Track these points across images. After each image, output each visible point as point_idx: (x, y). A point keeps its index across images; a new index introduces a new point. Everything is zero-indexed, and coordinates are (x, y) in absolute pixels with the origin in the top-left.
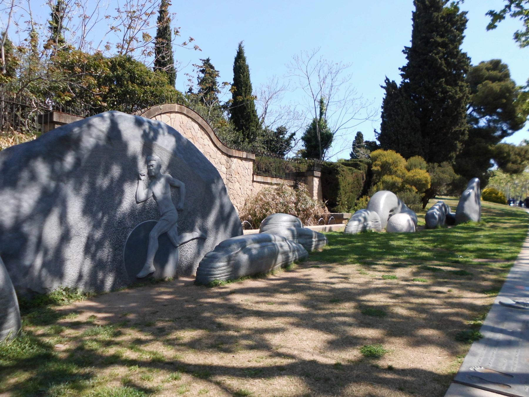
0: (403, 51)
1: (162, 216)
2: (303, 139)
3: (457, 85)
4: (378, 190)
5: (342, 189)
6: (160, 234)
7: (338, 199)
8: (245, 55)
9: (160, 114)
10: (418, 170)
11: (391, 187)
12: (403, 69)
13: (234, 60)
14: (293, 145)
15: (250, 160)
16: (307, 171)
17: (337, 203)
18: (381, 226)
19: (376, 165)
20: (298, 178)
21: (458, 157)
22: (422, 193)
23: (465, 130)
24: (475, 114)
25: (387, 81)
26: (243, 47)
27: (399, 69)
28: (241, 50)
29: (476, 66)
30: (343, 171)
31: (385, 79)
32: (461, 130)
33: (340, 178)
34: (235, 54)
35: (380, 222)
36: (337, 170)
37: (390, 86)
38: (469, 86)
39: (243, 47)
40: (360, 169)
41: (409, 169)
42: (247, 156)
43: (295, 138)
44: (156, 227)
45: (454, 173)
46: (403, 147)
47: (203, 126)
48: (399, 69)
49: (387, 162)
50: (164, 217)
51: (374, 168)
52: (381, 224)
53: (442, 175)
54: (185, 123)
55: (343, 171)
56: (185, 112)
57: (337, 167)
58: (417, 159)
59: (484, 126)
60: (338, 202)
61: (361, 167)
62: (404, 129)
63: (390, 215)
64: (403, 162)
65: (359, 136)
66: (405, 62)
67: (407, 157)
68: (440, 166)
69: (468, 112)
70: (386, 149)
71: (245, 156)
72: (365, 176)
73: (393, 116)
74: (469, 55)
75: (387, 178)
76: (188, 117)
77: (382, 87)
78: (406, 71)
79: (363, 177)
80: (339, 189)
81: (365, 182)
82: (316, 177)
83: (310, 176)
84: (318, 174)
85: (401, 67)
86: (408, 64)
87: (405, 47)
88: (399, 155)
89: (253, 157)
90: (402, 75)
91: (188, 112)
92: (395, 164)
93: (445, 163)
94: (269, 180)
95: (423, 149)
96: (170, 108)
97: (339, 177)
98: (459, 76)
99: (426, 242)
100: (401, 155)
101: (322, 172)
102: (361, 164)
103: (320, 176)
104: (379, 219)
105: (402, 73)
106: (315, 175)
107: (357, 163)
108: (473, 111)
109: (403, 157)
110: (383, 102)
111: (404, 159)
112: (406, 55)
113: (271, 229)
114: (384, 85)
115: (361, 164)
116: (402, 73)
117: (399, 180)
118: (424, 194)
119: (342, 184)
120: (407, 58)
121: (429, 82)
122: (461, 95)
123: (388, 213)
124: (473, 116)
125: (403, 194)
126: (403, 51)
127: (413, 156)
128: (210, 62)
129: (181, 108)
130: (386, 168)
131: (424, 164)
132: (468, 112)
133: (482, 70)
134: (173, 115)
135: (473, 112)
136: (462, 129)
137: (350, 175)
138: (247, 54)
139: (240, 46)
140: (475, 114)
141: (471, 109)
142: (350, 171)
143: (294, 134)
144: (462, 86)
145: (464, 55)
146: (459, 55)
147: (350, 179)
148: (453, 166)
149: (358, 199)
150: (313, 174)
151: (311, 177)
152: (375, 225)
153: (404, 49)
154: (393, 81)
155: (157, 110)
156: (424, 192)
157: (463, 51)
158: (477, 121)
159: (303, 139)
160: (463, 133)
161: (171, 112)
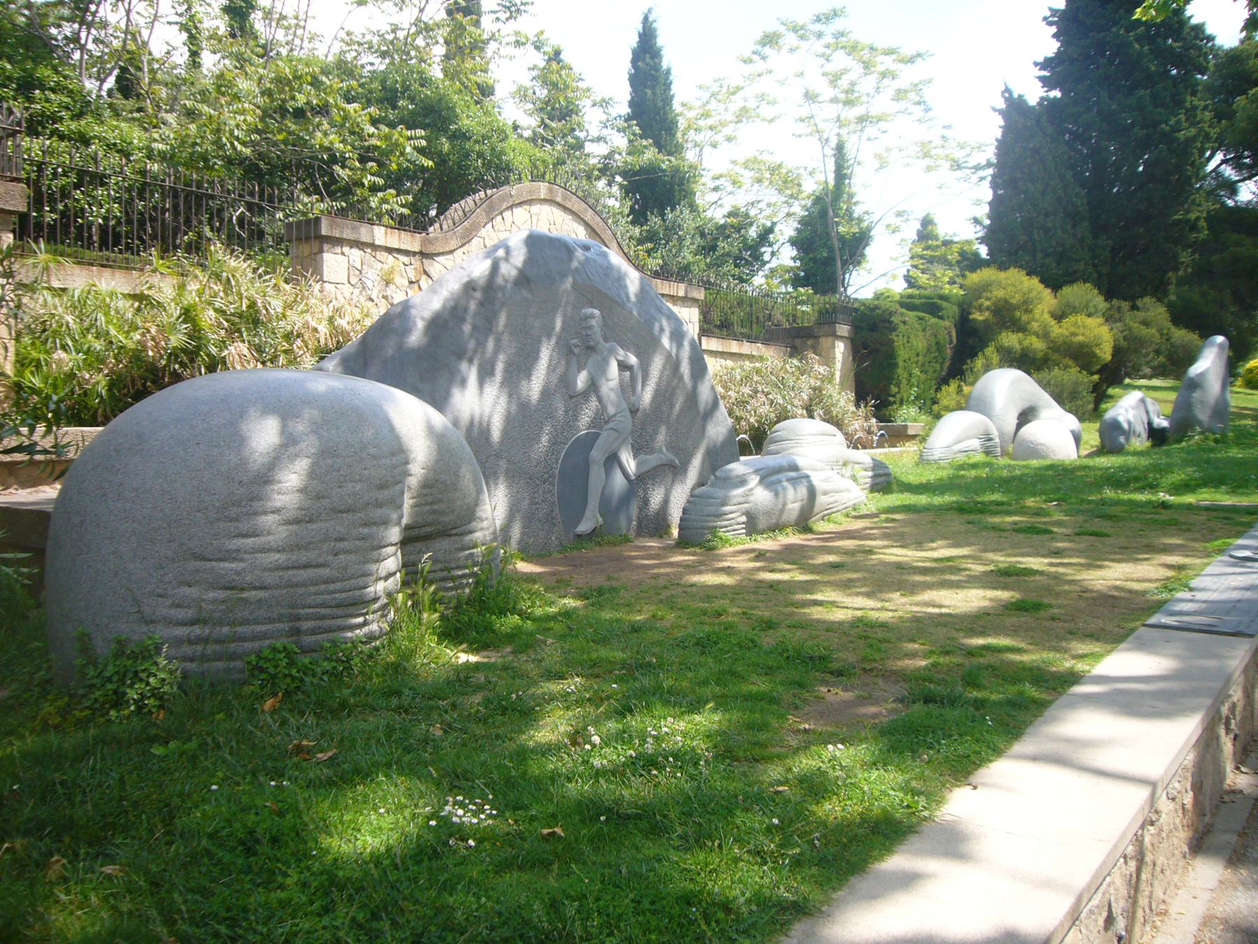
0: (1045, 19)
1: (607, 422)
2: (793, 242)
3: (1179, 103)
4: (988, 368)
5: (901, 364)
6: (606, 455)
7: (894, 389)
8: (660, 41)
9: (511, 207)
10: (1081, 319)
11: (1025, 362)
12: (1047, 64)
13: (630, 56)
14: (766, 257)
15: (695, 301)
16: (819, 323)
17: (892, 399)
18: (999, 449)
19: (980, 309)
20: (798, 342)
21: (1180, 283)
22: (1092, 374)
23: (1198, 218)
24: (1228, 171)
25: (1007, 95)
26: (655, 21)
27: (1036, 64)
28: (650, 28)
29: (1232, 50)
30: (904, 323)
31: (1004, 88)
32: (1189, 221)
33: (899, 342)
34: (634, 40)
35: (997, 440)
36: (891, 322)
37: (1015, 108)
38: (1210, 107)
39: (655, 21)
40: (941, 318)
41: (1059, 317)
42: (686, 293)
43: (165, 48)
44: (600, 442)
45: (1170, 325)
46: (1047, 261)
47: (595, 227)
48: (1036, 64)
49: (1006, 301)
50: (610, 425)
51: (978, 316)
52: (999, 445)
53: (1144, 332)
54: (559, 222)
55: (904, 323)
56: (558, 199)
57: (891, 314)
58: (1080, 292)
59: (1250, 202)
60: (894, 396)
61: (945, 312)
62: (1046, 215)
63: (1020, 426)
64: (1046, 300)
65: (926, 232)
66: (1051, 47)
67: (1054, 285)
68: (1134, 308)
69: (1211, 166)
70: (1003, 267)
71: (681, 293)
72: (954, 334)
73: (1020, 184)
74: (1209, 31)
75: (1010, 339)
76: (565, 209)
77: (994, 110)
78: (1055, 70)
79: (950, 336)
80: (895, 365)
81: (954, 347)
82: (841, 338)
83: (826, 336)
84: (844, 330)
85: (1041, 60)
86: (1058, 54)
87: (1050, 9)
88: (1035, 282)
89: (700, 294)
90: (1041, 79)
91: (565, 198)
92: (1027, 306)
93: (1147, 300)
94: (734, 347)
95: (1095, 266)
96: (530, 192)
97: (895, 338)
98: (1185, 81)
99: (1079, 568)
100: (1042, 281)
101: (856, 328)
102: (944, 304)
103: (846, 334)
104: (995, 434)
105: (1045, 73)
106: (838, 334)
107: (935, 303)
108: (1223, 162)
109: (1047, 286)
110: (997, 148)
111: (1048, 291)
112: (1054, 29)
113: (787, 449)
114: (1002, 105)
115: (944, 304)
116: (1045, 73)
117: (1037, 345)
118: (1096, 377)
119: (902, 354)
120: (1055, 36)
121: (1111, 97)
122: (1193, 131)
123: (1015, 421)
124: (1222, 176)
125: (1044, 374)
126: (1045, 19)
127: (1071, 282)
128: (562, 56)
129: (550, 190)
130: (1007, 316)
131: (1100, 302)
132: (1211, 166)
133: (1248, 57)
134: (535, 208)
135: (1224, 166)
136: (1192, 216)
137: (920, 333)
138: (662, 40)
139: (646, 19)
140: (1228, 171)
141: (1219, 157)
142: (920, 324)
143: (770, 230)
144: (1194, 108)
145: (1199, 29)
146: (1186, 30)
147: (920, 343)
148: (1171, 307)
149: (938, 389)
150: (835, 331)
151: (830, 339)
152: (987, 447)
153: (1048, 14)
154: (1020, 96)
155: (503, 199)
156: (1097, 372)
157: (1194, 21)
158: (1232, 188)
159: (793, 242)
160: (1194, 227)
161: (530, 202)
